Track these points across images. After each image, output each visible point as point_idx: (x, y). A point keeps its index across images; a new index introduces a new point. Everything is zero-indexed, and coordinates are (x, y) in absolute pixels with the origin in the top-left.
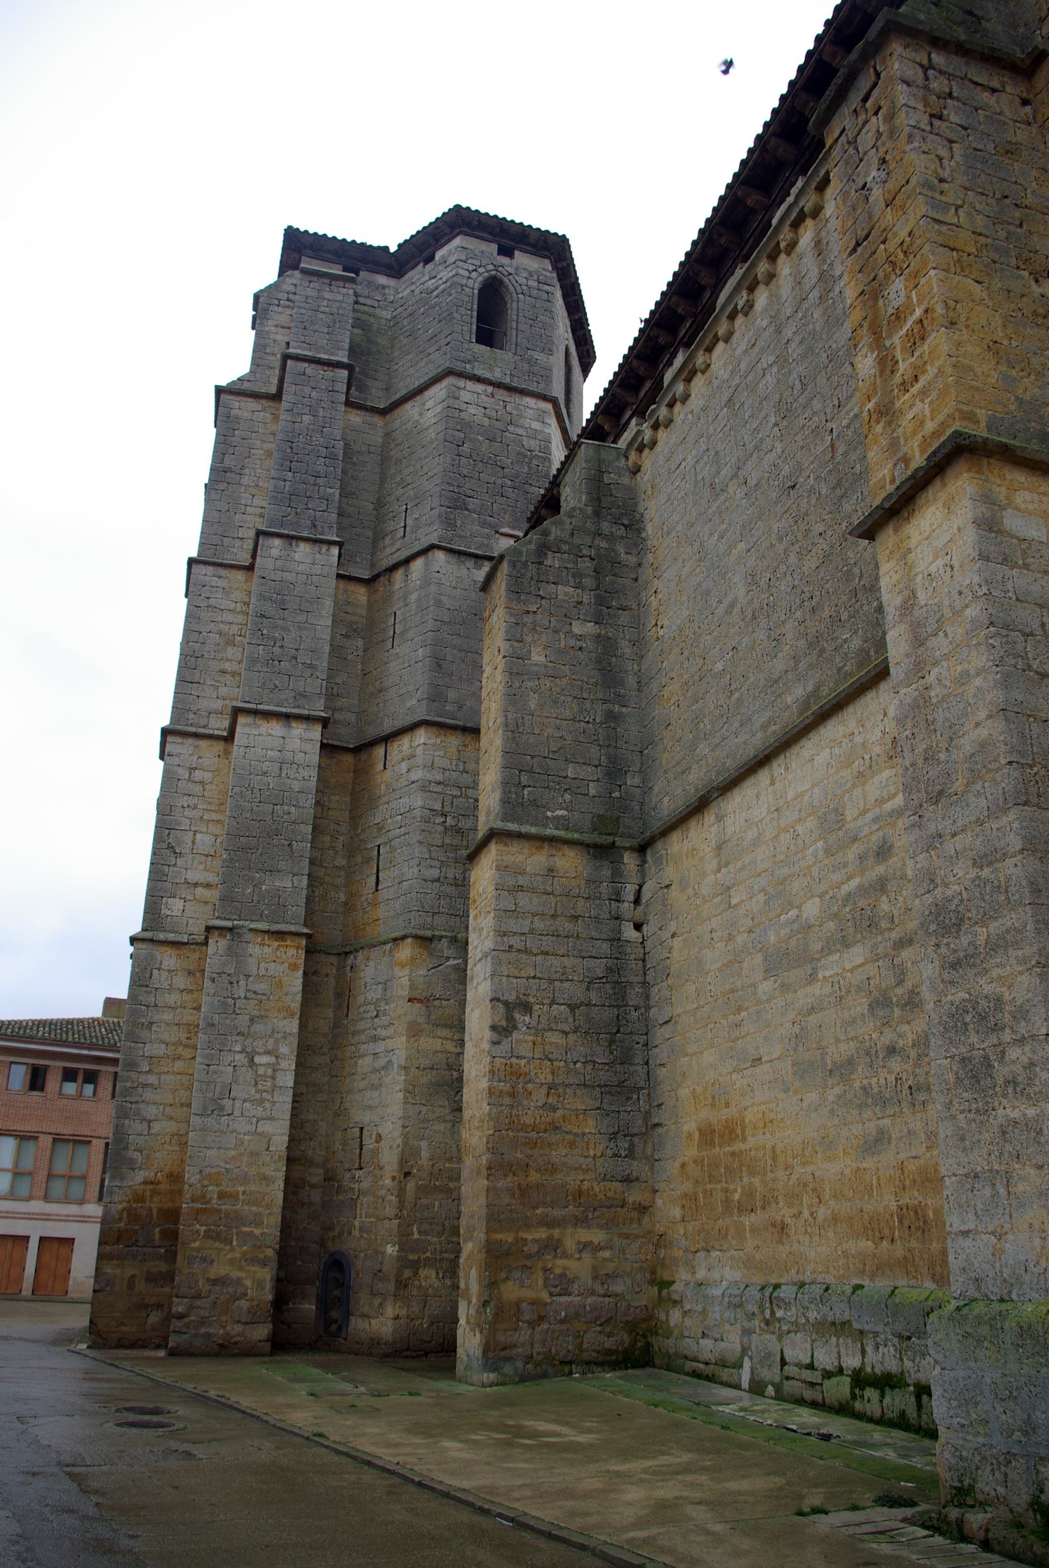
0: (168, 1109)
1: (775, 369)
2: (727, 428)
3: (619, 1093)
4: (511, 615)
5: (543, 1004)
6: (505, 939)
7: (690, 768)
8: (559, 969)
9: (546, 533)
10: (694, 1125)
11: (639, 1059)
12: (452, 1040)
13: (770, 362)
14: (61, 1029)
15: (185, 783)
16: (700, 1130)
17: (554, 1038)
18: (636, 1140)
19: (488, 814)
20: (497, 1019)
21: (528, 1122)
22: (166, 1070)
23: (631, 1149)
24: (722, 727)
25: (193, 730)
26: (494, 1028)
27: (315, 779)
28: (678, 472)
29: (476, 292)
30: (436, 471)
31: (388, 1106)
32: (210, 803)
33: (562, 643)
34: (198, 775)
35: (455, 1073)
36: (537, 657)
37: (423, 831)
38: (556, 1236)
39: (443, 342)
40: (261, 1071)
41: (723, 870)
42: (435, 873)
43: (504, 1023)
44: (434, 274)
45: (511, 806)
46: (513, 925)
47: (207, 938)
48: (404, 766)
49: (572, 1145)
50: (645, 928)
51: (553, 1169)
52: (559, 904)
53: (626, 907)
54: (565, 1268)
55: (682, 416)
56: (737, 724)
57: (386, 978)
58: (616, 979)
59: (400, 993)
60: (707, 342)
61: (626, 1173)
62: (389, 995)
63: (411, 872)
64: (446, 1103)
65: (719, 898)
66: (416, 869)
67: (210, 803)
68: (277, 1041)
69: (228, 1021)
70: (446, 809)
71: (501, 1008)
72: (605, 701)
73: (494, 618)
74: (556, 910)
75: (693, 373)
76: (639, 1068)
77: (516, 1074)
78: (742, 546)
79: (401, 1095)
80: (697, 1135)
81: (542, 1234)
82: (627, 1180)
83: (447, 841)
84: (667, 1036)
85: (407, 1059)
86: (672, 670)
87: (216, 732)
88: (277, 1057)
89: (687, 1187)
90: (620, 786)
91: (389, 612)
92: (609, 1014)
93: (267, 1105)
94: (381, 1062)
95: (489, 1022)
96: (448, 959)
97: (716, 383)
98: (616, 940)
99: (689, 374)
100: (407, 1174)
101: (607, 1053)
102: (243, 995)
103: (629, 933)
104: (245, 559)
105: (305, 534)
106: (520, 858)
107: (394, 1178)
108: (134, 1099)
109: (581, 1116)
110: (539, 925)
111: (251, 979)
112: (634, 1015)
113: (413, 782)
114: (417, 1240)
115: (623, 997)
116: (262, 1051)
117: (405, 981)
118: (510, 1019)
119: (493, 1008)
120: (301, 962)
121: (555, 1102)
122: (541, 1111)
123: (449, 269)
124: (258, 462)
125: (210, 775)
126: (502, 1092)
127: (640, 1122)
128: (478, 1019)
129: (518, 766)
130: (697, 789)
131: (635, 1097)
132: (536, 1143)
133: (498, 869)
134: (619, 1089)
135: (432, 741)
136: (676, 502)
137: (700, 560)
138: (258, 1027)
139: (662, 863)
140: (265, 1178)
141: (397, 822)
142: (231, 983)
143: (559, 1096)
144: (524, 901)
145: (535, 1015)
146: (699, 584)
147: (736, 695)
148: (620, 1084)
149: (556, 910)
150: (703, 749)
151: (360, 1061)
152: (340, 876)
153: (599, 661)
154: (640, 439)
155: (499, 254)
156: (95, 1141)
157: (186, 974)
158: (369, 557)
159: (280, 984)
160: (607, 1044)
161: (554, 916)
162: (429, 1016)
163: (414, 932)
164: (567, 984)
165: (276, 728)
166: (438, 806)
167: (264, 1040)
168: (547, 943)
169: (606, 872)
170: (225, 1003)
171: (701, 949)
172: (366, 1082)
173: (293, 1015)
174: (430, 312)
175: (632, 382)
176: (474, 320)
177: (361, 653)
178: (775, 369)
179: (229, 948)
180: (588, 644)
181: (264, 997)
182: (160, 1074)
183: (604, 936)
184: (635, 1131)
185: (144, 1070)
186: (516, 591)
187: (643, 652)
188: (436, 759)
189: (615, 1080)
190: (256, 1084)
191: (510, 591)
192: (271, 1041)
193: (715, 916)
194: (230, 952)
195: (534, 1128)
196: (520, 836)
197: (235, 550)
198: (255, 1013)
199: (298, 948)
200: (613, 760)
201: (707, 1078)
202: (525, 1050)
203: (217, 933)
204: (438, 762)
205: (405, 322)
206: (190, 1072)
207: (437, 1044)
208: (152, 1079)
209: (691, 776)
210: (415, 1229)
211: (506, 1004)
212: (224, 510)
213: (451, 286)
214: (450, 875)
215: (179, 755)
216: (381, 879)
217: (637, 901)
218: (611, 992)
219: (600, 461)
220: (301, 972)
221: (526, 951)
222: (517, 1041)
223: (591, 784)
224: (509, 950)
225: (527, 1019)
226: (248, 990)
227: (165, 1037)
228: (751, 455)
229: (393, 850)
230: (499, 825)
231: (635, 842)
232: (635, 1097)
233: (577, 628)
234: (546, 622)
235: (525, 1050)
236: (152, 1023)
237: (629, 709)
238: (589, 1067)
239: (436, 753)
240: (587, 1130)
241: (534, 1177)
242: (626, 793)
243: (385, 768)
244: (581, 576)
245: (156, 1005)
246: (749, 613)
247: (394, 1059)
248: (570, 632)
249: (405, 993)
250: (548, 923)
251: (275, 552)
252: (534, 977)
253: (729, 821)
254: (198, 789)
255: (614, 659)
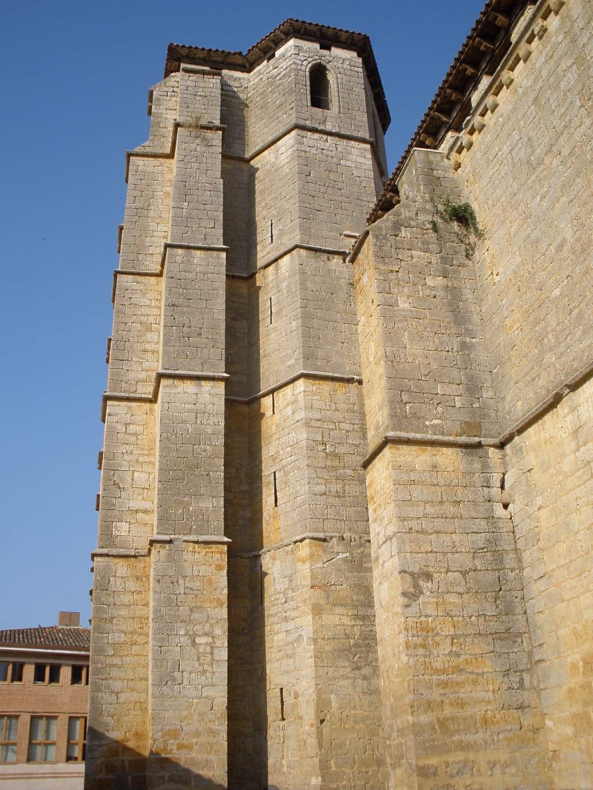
0: (130, 683)
1: (575, 68)
2: (537, 118)
3: (507, 638)
4: (380, 274)
5: (441, 573)
6: (406, 523)
7: (539, 375)
8: (449, 544)
9: (398, 214)
10: (577, 657)
11: (519, 610)
12: (347, 616)
13: (569, 64)
14: (31, 635)
15: (123, 435)
16: (586, 662)
17: (453, 599)
18: (525, 675)
19: (377, 428)
20: (406, 587)
21: (439, 667)
22: (126, 653)
23: (521, 682)
24: (566, 338)
25: (127, 395)
26: (404, 594)
27: (223, 424)
28: (495, 160)
29: (308, 73)
30: (291, 194)
31: (302, 670)
32: (142, 449)
33: (421, 294)
34: (132, 429)
35: (352, 641)
36: (404, 304)
37: (310, 457)
38: (471, 759)
39: (288, 108)
40: (201, 649)
41: (582, 449)
42: (321, 488)
43: (412, 590)
44: (276, 65)
45: (398, 418)
46: (411, 512)
47: (150, 550)
48: (289, 410)
49: (475, 682)
50: (510, 507)
51: (461, 704)
52: (444, 493)
53: (496, 491)
54: (481, 784)
55: (493, 121)
56: (579, 333)
57: (290, 572)
58: (494, 548)
59: (304, 583)
60: (510, 62)
61: (520, 702)
62: (294, 585)
63: (303, 490)
64: (347, 664)
65: (581, 471)
66: (307, 487)
67: (142, 449)
68: (212, 626)
69: (173, 612)
70: (325, 439)
71: (408, 578)
72: (458, 335)
73: (365, 279)
74: (442, 498)
75: (500, 87)
76: (520, 617)
77: (426, 629)
78: (564, 200)
79: (312, 661)
80: (581, 664)
81: (460, 756)
82: (521, 707)
83: (329, 463)
84: (543, 589)
85: (314, 633)
86: (512, 304)
87: (143, 396)
88: (213, 638)
89: (577, 708)
90: (479, 399)
91: (266, 298)
92: (492, 576)
93: (209, 675)
94: (293, 636)
95: (400, 590)
96: (338, 553)
97: (520, 91)
98: (490, 518)
99: (496, 88)
100: (322, 721)
101: (494, 607)
102: (182, 592)
103: (499, 511)
104: (157, 269)
105: (200, 245)
106: (409, 459)
107: (312, 725)
108: (104, 677)
109: (480, 659)
110: (430, 509)
111: (187, 578)
112: (512, 575)
113: (298, 421)
114: (335, 771)
115: (501, 562)
116: (201, 633)
117: (307, 573)
118: (416, 586)
119: (402, 578)
120: (225, 563)
121: (458, 650)
122: (448, 657)
123: (287, 60)
124: (160, 201)
125: (141, 427)
126: (415, 644)
127: (526, 660)
128: (386, 589)
129: (400, 387)
130: (548, 390)
131: (519, 640)
132: (447, 683)
133: (394, 468)
134: (506, 635)
135: (310, 389)
136: (497, 182)
137: (526, 218)
138: (196, 615)
139: (523, 453)
140: (211, 732)
141: (288, 453)
142: (172, 583)
143: (461, 645)
144: (417, 492)
145: (435, 581)
146: (529, 236)
147: (576, 311)
148: (507, 631)
149: (442, 498)
150: (550, 358)
151: (276, 638)
152: (245, 498)
153: (450, 304)
154: (459, 143)
155: (321, 49)
156: (61, 715)
157: (135, 579)
158: (246, 261)
159: (210, 582)
160: (493, 600)
161: (441, 502)
162: (328, 598)
163: (311, 535)
164: (457, 556)
165: (189, 387)
166: (319, 438)
167: (202, 625)
168: (439, 524)
169: (477, 466)
170: (169, 599)
171: (568, 515)
172: (282, 653)
173: (221, 605)
174: (276, 90)
175: (446, 106)
176: (308, 92)
177: (246, 331)
178: (575, 68)
179: (169, 556)
180: (440, 293)
181: (199, 592)
182: (122, 656)
183: (481, 515)
184: (521, 667)
185: (110, 654)
186: (381, 257)
187: (482, 297)
188: (314, 402)
189: (502, 629)
190: (199, 659)
191: (376, 255)
192: (207, 625)
193: (579, 486)
194: (170, 559)
195: (444, 671)
196: (409, 442)
197: (148, 263)
198: (193, 604)
199: (221, 553)
200: (471, 378)
201: (585, 617)
202: (431, 610)
203: (158, 545)
204: (316, 404)
205: (258, 99)
206: (145, 654)
207: (336, 620)
208: (116, 661)
209: (541, 382)
210: (332, 763)
211: (412, 574)
212: (137, 235)
213: (290, 71)
214: (333, 489)
215: (116, 415)
216: (278, 497)
217: (502, 487)
218: (492, 558)
219: (430, 162)
220: (226, 571)
221: (423, 532)
222: (424, 603)
223: (457, 398)
224: (409, 532)
225: (429, 584)
226: (185, 588)
227: (124, 628)
228: (562, 133)
229: (286, 474)
230: (391, 434)
231: (496, 441)
232: (519, 640)
233: (430, 282)
234: (406, 278)
235: (431, 610)
236: (113, 618)
237: (478, 340)
238: (482, 619)
239: (314, 398)
240: (486, 670)
241: (448, 711)
242: (484, 403)
243: (274, 413)
244: (428, 243)
245: (115, 604)
246: (578, 247)
247: (303, 633)
248: (425, 284)
249: (308, 582)
250: (437, 508)
251: (179, 259)
252: (431, 552)
253: (582, 410)
254: (133, 439)
255: (461, 303)
